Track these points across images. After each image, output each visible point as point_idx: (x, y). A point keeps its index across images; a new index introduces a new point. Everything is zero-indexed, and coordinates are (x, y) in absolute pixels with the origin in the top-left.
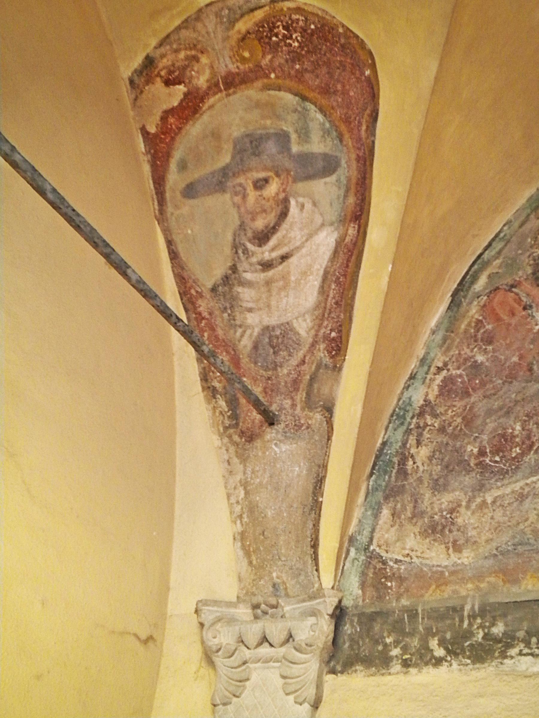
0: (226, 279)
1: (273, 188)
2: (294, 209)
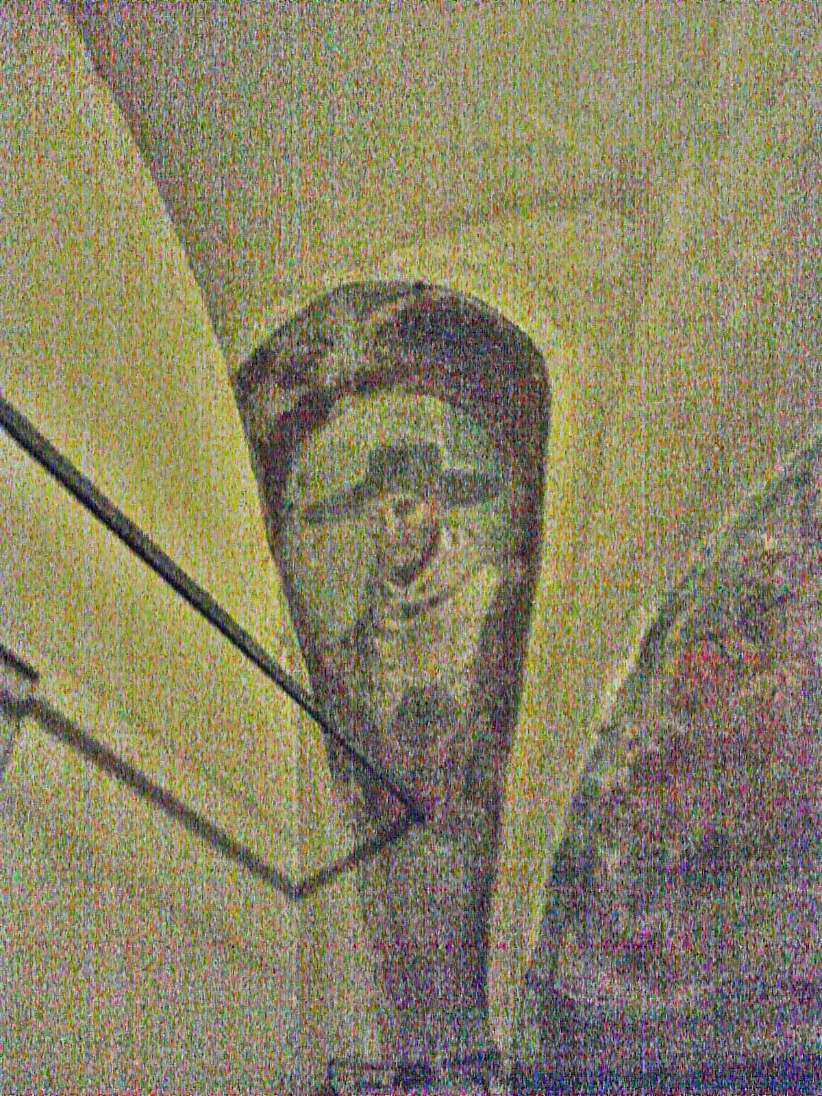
0: (360, 628)
1: (419, 514)
2: (445, 541)
